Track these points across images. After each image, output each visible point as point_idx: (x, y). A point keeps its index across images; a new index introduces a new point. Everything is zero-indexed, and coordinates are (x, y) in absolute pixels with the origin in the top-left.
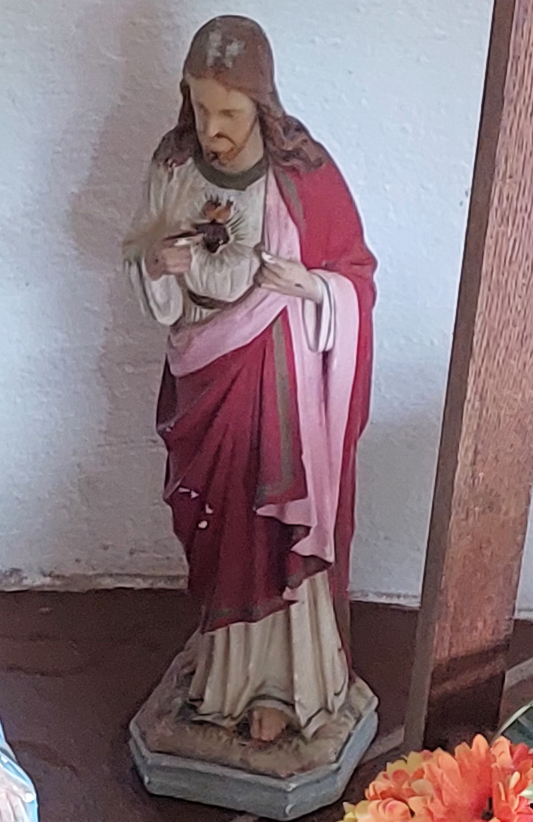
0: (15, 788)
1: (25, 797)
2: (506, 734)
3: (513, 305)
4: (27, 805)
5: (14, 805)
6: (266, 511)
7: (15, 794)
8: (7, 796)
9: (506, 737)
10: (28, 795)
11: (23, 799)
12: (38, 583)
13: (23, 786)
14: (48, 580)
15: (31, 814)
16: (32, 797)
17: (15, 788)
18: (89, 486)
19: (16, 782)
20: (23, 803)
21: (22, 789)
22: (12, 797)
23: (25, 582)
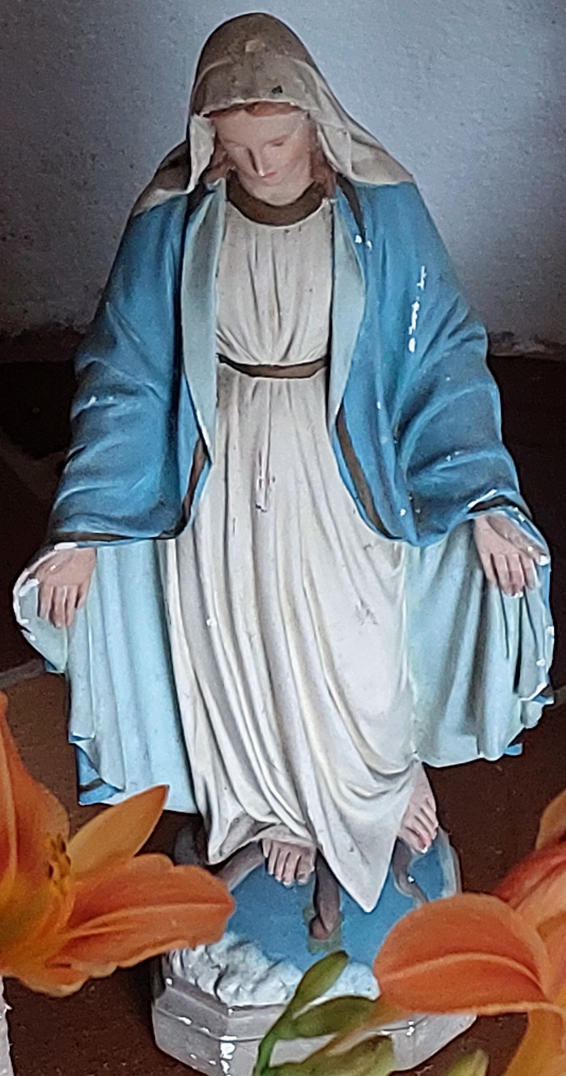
0: (530, 549)
1: (540, 561)
2: (170, 851)
3: (408, 672)
4: (540, 569)
5: (526, 567)
6: (241, 787)
7: (529, 555)
8: (520, 558)
9: (173, 849)
10: (543, 558)
11: (537, 561)
12: (532, 349)
13: (536, 548)
14: (541, 348)
15: (543, 577)
16: (545, 560)
17: (530, 549)
18: (298, 652)
19: (531, 542)
20: (536, 565)
21: (537, 551)
22: (525, 559)
23: (517, 347)
